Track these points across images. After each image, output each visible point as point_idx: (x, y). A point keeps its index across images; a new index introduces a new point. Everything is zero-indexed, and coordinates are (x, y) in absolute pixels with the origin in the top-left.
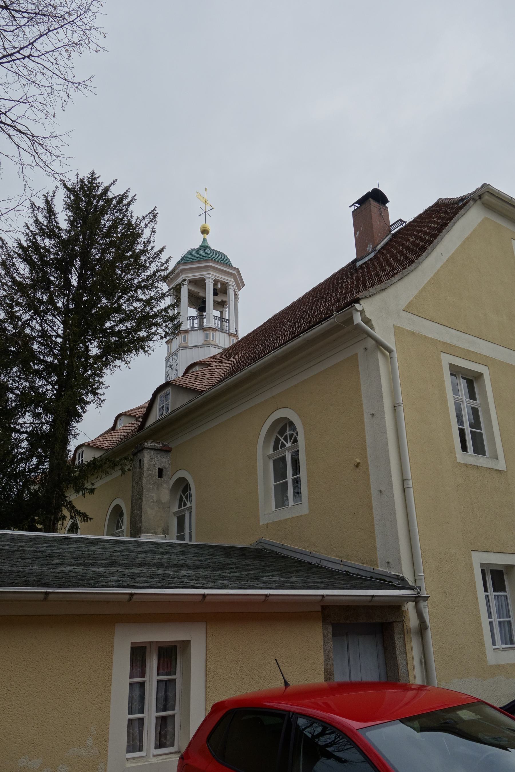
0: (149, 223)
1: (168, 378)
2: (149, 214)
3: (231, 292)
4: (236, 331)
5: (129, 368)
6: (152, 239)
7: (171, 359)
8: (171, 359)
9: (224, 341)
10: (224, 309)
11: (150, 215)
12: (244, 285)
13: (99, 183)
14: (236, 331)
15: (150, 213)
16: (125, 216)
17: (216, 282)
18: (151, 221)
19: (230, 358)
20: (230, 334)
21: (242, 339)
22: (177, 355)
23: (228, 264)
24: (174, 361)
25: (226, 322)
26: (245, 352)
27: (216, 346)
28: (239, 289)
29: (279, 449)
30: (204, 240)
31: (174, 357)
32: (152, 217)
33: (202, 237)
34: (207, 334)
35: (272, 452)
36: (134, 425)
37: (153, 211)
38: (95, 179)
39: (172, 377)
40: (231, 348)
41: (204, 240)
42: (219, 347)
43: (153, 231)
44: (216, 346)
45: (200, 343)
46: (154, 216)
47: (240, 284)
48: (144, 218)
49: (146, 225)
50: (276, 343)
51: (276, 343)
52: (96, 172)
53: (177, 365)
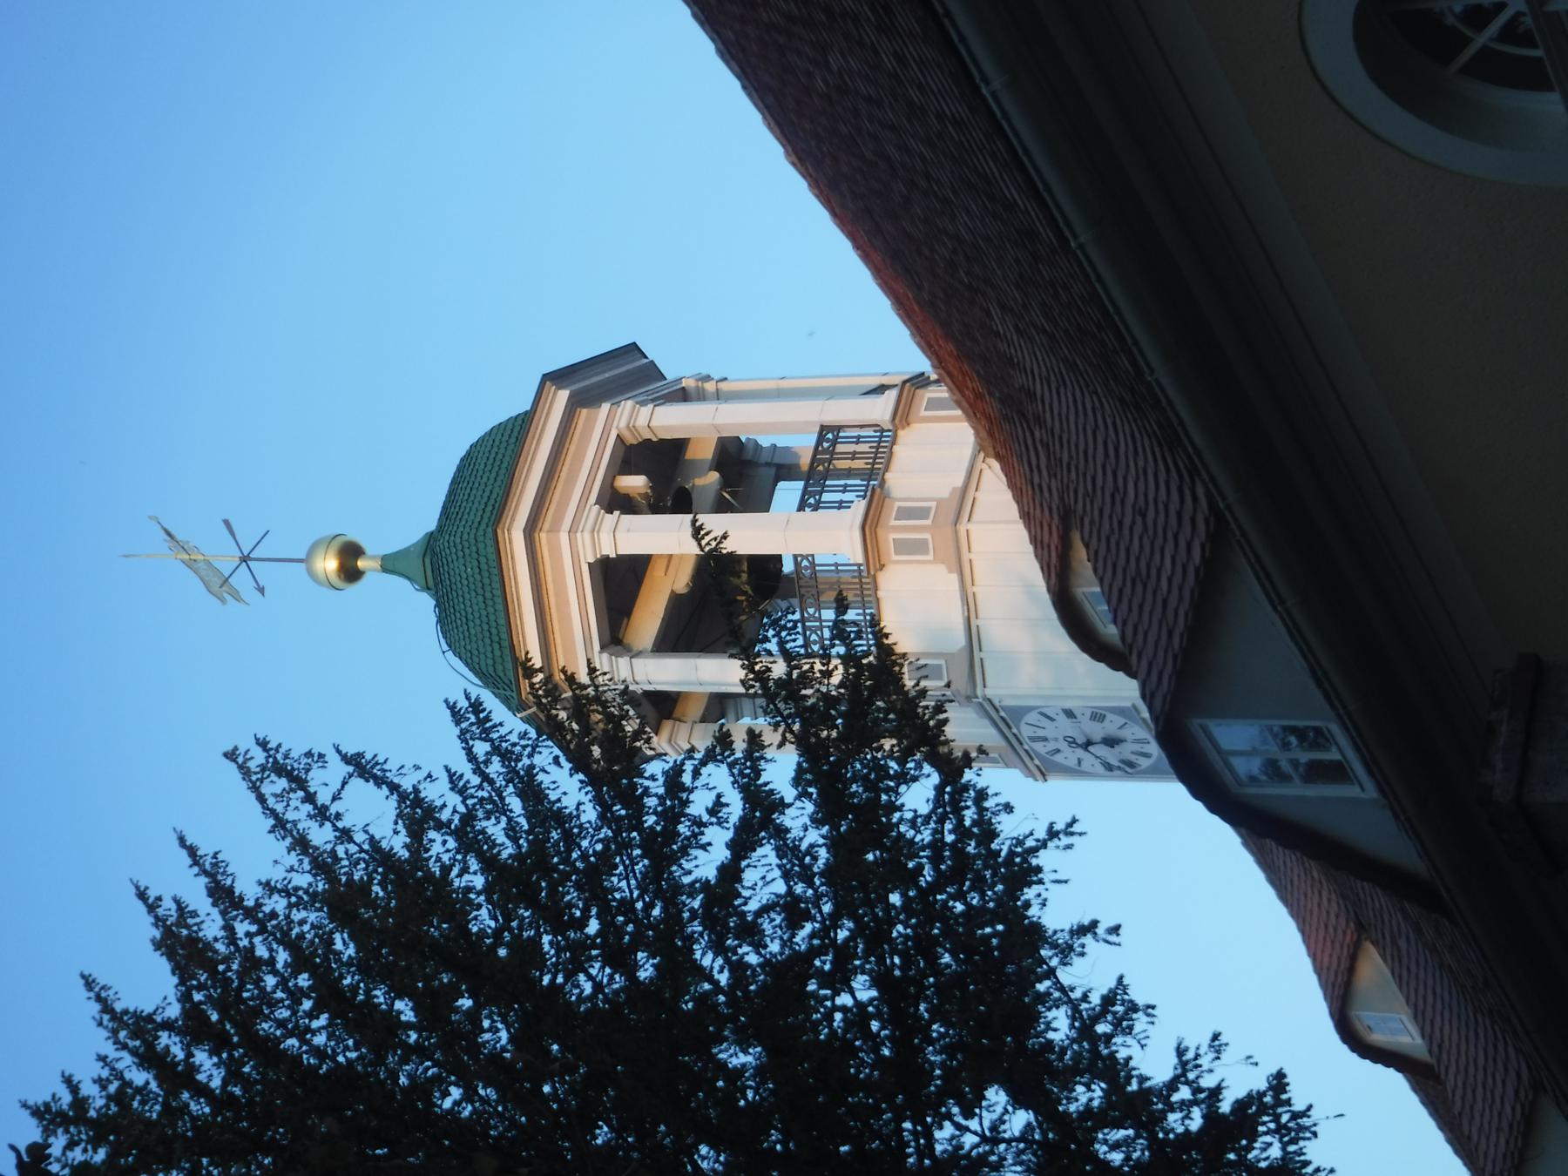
0: (310, 798)
1: (1144, 763)
2: (261, 799)
3: (668, 420)
4: (881, 389)
5: (1115, 930)
6: (407, 784)
7: (1039, 747)
8: (1039, 747)
9: (942, 450)
10: (764, 458)
11: (267, 789)
12: (633, 349)
13: (102, 1083)
14: (881, 389)
15: (255, 788)
16: (286, 934)
17: (616, 502)
18: (298, 782)
19: (1031, 395)
20: (902, 415)
21: (927, 344)
22: (1018, 713)
23: (517, 431)
24: (1049, 730)
25: (834, 443)
26: (995, 311)
27: (962, 503)
28: (652, 373)
29: (1539, 53)
30: (390, 564)
31: (1026, 732)
32: (283, 783)
33: (374, 581)
34: (904, 547)
35: (1555, 97)
36: (1402, 943)
37: (245, 771)
38: (80, 1103)
39: (1142, 740)
40: (975, 409)
41: (390, 564)
42: (972, 477)
43: (362, 767)
44: (962, 503)
45: (954, 579)
46: (276, 772)
47: (622, 372)
48: (280, 825)
49: (322, 814)
50: (940, 117)
51: (940, 117)
52: (40, 1097)
53: (1069, 714)
